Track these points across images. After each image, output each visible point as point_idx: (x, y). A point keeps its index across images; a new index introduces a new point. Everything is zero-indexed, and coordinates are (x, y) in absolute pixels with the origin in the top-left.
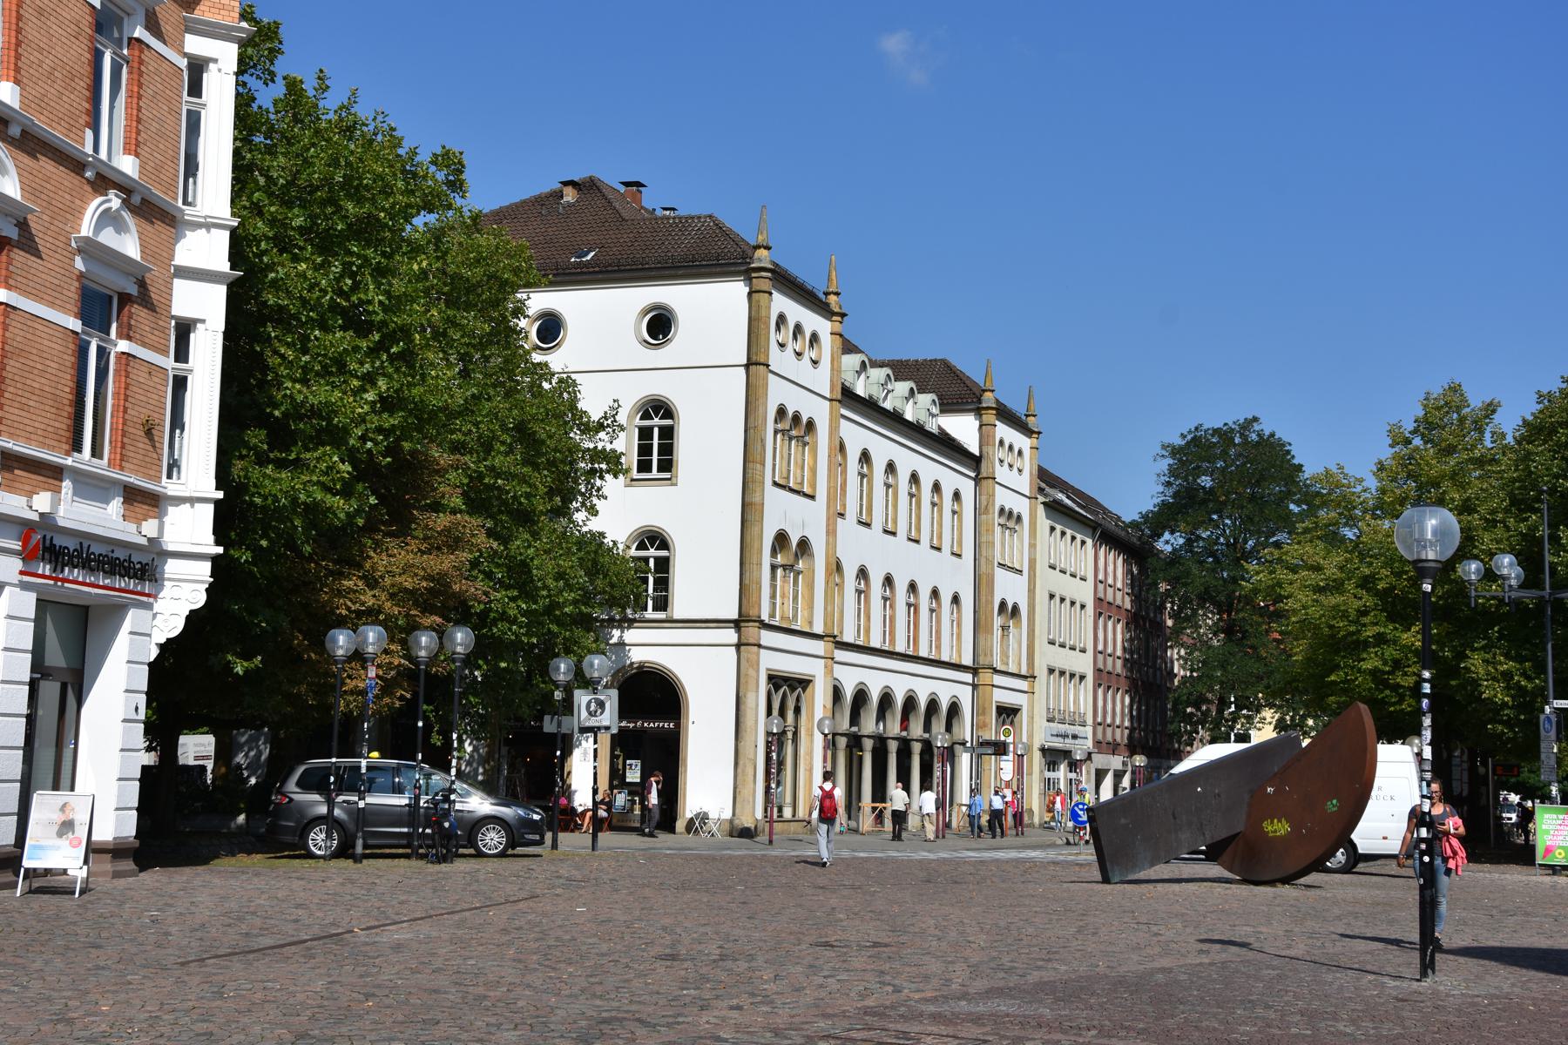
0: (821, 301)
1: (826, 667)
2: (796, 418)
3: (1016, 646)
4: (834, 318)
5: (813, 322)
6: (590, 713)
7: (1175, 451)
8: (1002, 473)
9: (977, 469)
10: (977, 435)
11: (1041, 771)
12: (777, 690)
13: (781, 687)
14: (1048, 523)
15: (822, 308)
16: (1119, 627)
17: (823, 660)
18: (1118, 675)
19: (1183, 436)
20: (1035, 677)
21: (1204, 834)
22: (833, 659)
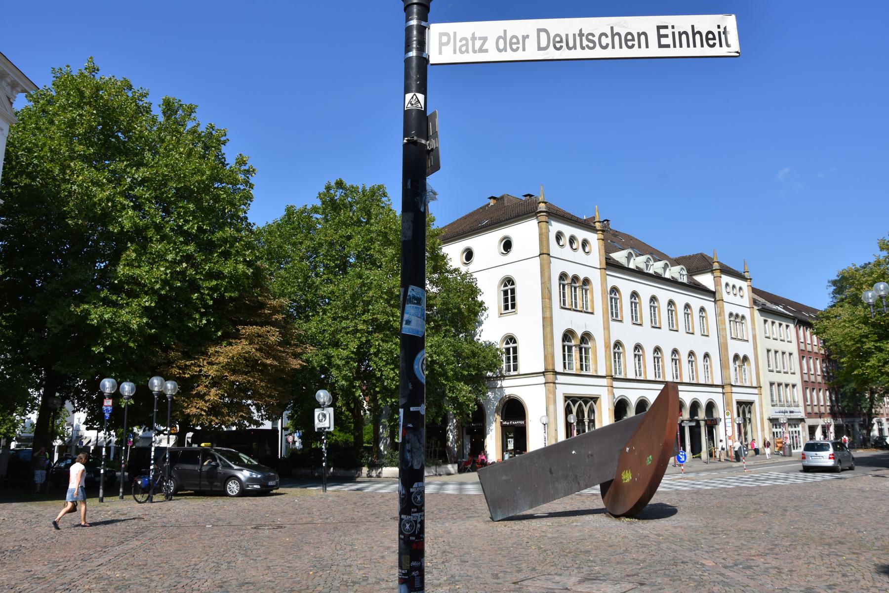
0: (592, 226)
1: (608, 390)
2: (737, 316)
3: (749, 374)
4: (598, 232)
5: (738, 283)
6: (319, 421)
7: (834, 283)
8: (726, 297)
9: (714, 297)
10: (713, 282)
11: (770, 429)
12: (741, 406)
13: (577, 401)
14: (762, 319)
15: (587, 225)
16: (818, 362)
17: (607, 388)
18: (819, 383)
19: (838, 276)
20: (761, 387)
21: (579, 483)
22: (612, 387)
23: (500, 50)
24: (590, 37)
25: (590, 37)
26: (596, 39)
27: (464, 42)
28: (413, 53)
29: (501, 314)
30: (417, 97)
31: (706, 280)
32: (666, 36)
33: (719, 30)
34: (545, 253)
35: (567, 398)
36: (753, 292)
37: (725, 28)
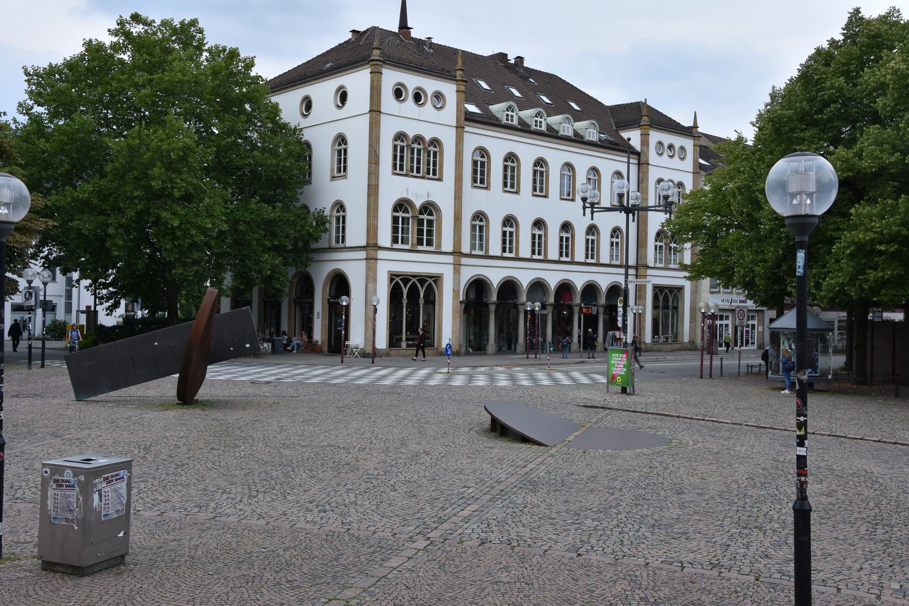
29: (333, 177)
31: (634, 137)
34: (375, 111)
35: (393, 276)
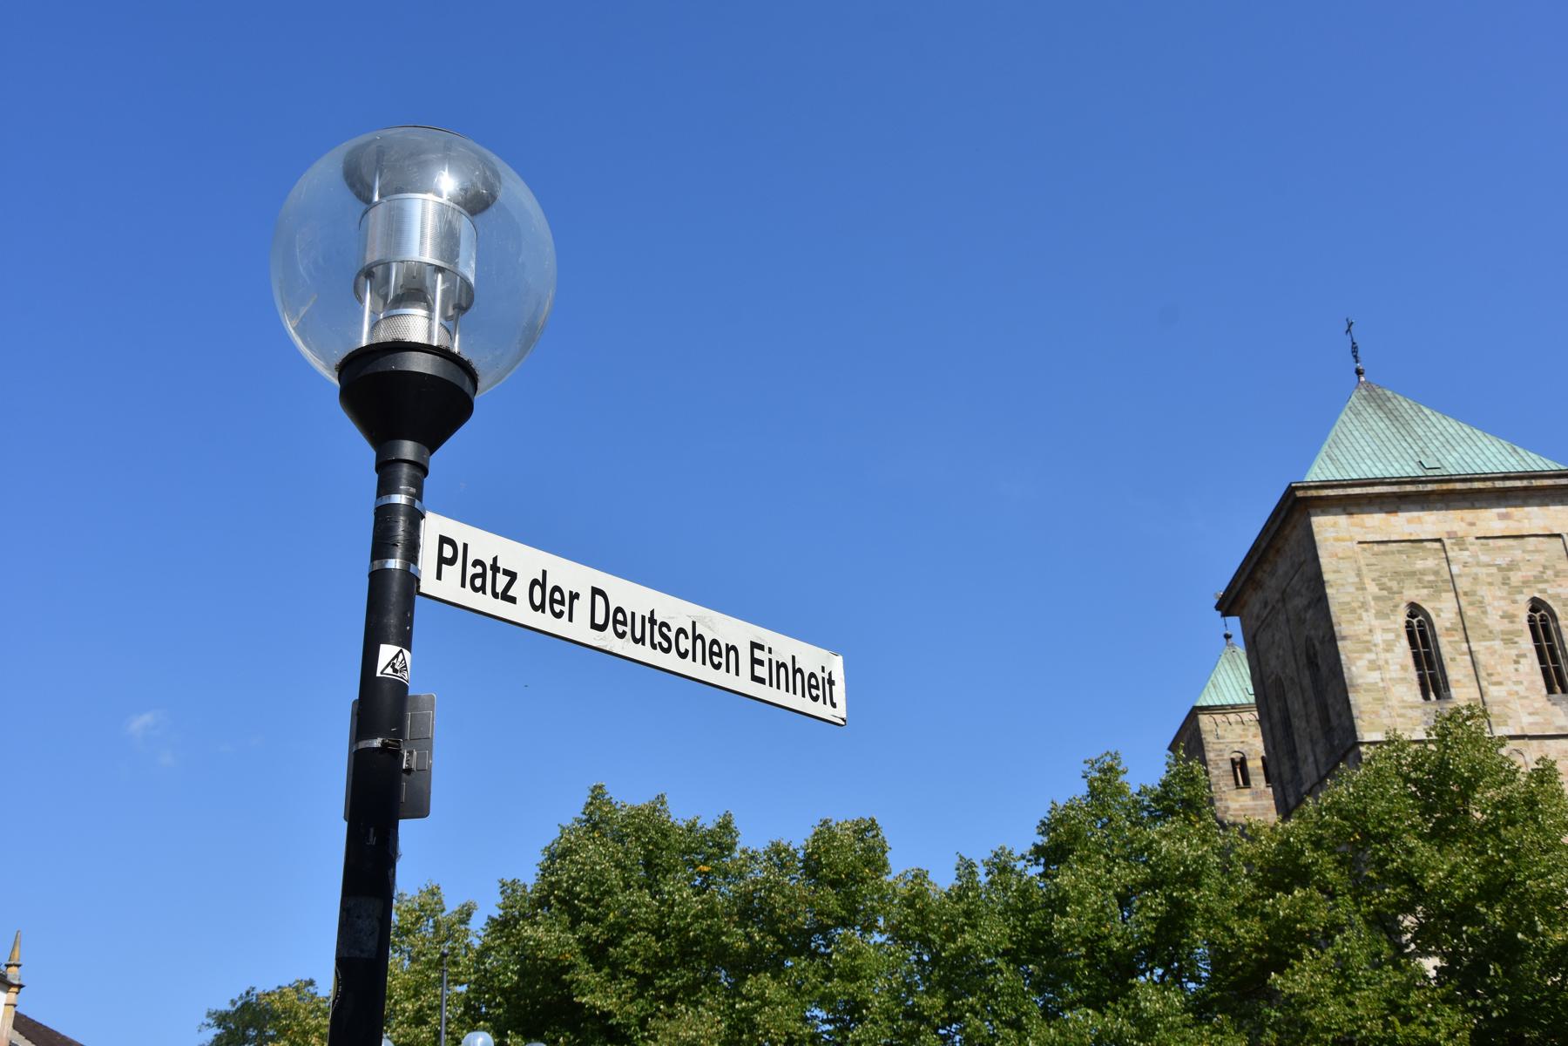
7: (221, 1019)
23: (594, 626)
24: (664, 630)
25: (664, 630)
26: (672, 635)
27: (479, 570)
28: (395, 564)
30: (404, 659)
32: (761, 663)
33: (823, 675)
36: (15, 1027)
37: (830, 674)
